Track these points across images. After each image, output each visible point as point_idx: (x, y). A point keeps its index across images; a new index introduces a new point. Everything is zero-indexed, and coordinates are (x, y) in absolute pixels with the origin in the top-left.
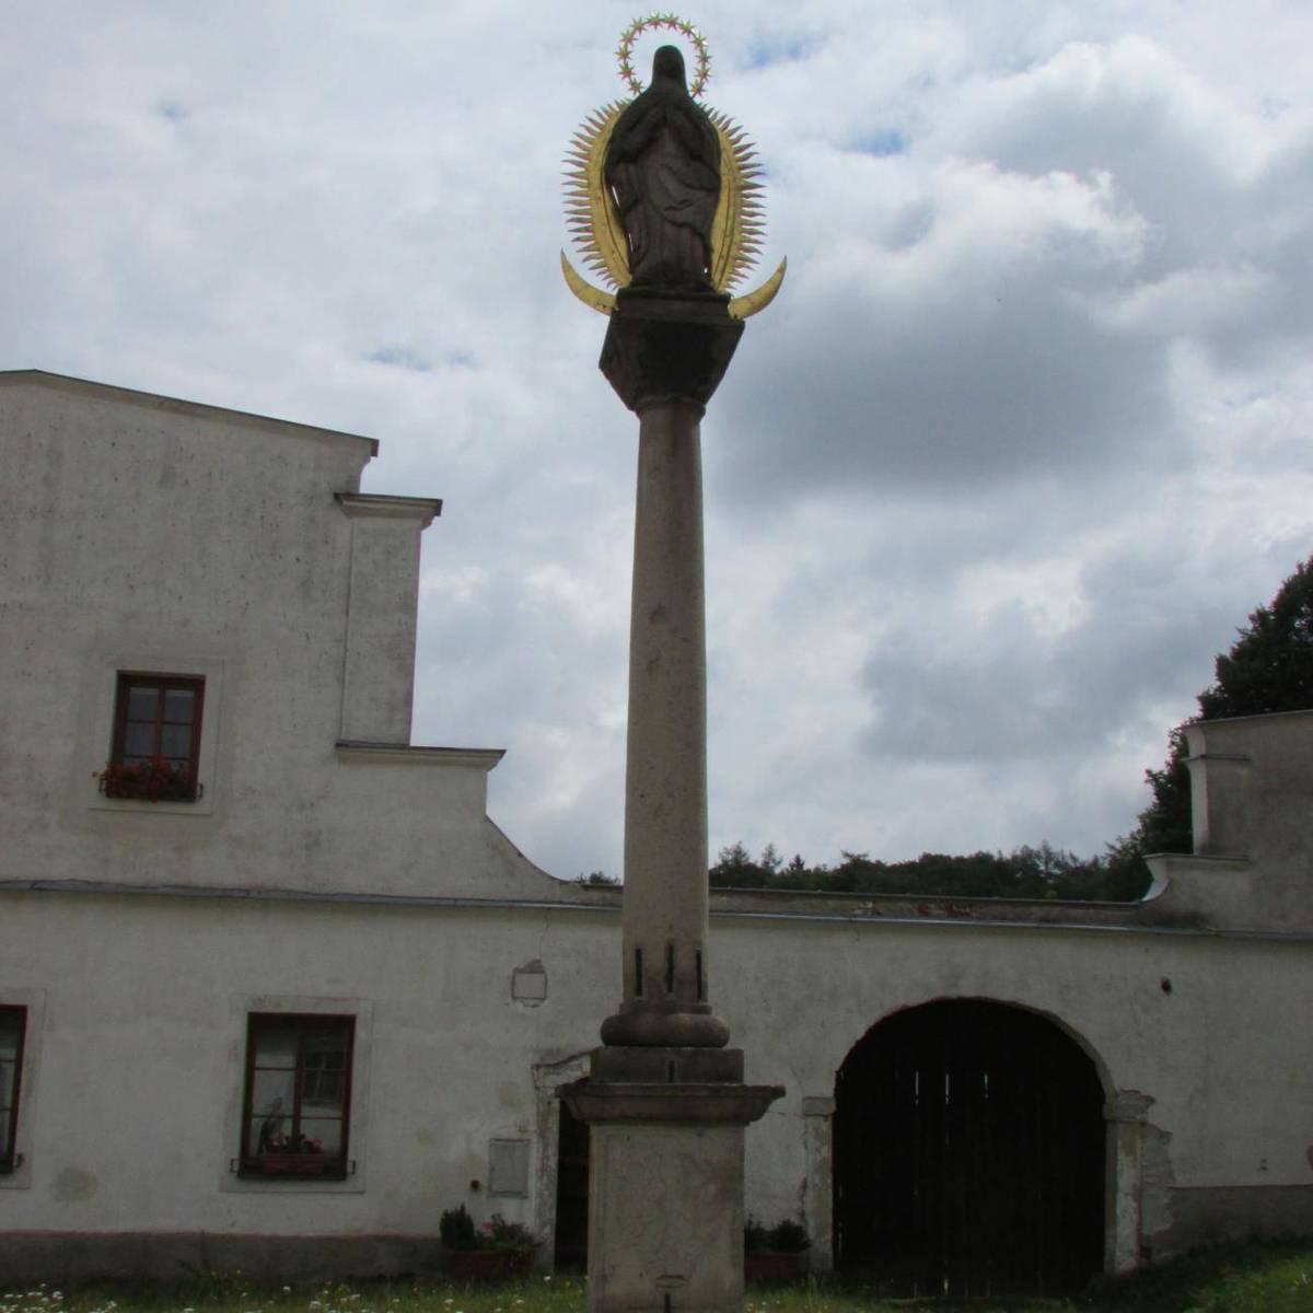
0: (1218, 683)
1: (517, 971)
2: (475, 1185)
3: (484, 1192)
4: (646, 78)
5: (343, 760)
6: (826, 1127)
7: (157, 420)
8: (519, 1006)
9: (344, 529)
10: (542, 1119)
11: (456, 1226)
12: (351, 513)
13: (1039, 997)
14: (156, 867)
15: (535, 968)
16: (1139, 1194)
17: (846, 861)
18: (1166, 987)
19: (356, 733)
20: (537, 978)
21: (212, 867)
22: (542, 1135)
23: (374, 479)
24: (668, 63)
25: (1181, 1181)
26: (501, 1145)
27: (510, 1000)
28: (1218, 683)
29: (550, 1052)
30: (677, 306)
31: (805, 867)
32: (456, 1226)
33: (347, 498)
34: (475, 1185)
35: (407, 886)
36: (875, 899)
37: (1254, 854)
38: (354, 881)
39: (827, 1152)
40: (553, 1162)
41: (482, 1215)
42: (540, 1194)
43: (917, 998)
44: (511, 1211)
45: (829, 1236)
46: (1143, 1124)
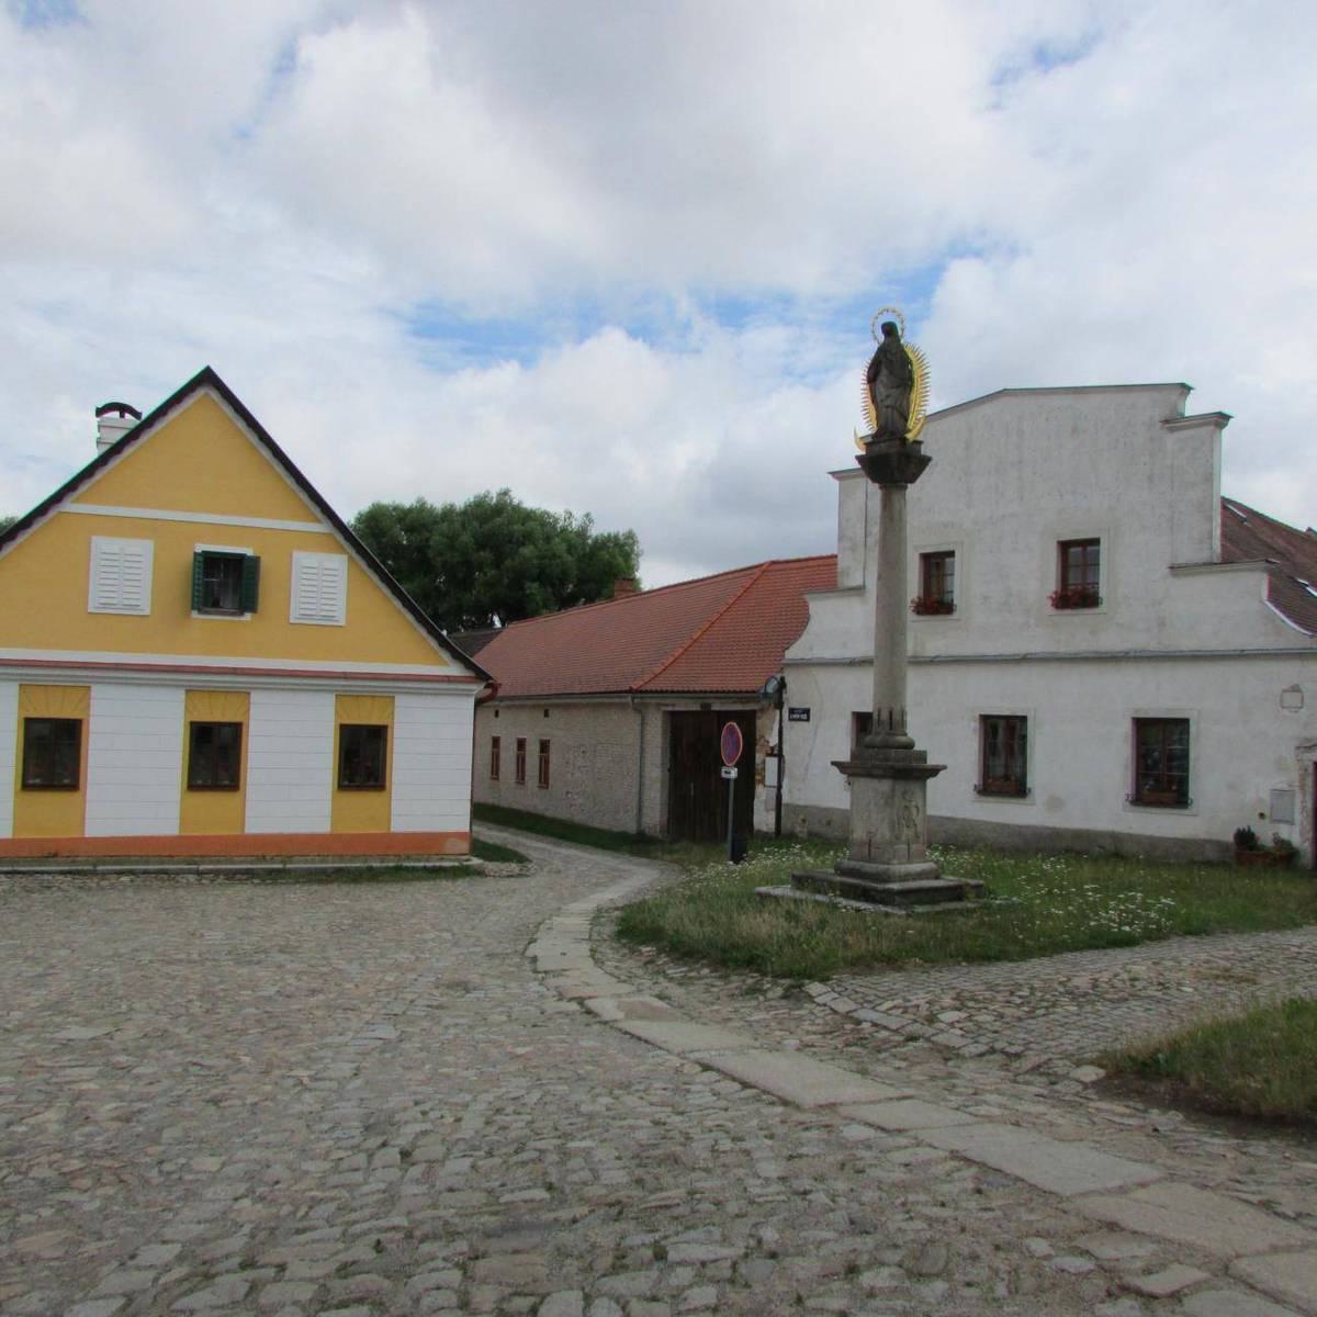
1: (1285, 691)
4: (882, 338)
5: (1175, 575)
7: (1067, 400)
8: (1286, 712)
9: (1171, 441)
12: (1172, 430)
14: (1082, 643)
15: (1295, 689)
19: (1181, 560)
20: (1298, 695)
21: (1110, 641)
22: (1302, 787)
24: (889, 330)
27: (1280, 709)
40: (1309, 805)
42: (1302, 823)
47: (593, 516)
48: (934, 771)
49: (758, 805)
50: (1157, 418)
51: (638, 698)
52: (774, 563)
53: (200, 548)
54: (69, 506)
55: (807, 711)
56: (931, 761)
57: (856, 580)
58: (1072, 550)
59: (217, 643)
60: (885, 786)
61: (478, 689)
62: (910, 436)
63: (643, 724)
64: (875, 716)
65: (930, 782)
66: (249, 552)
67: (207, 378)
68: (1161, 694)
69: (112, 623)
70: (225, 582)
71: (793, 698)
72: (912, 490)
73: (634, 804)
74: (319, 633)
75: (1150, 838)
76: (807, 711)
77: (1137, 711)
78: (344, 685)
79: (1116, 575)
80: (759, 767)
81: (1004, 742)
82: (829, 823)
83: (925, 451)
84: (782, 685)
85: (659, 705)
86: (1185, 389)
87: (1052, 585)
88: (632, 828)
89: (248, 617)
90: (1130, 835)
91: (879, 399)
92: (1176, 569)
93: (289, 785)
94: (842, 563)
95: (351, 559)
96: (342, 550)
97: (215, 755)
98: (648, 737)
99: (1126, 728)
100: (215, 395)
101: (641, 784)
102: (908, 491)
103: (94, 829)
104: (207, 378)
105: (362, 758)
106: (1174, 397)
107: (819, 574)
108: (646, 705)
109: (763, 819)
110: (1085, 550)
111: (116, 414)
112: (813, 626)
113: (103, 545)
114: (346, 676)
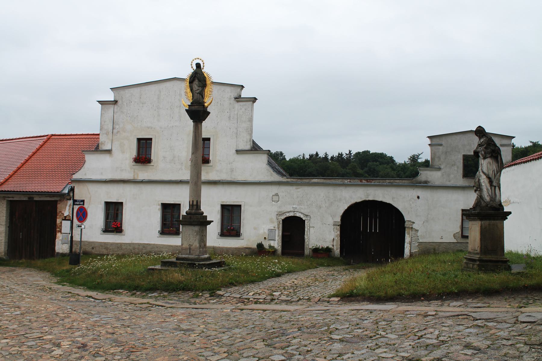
0: (288, 159)
2: (265, 238)
3: (267, 239)
4: (195, 68)
5: (237, 154)
6: (339, 227)
10: (278, 225)
11: (260, 246)
12: (238, 102)
13: (387, 200)
15: (277, 195)
16: (410, 243)
17: (531, 144)
18: (418, 197)
19: (240, 148)
22: (278, 228)
23: (245, 94)
24: (198, 66)
25: (420, 241)
26: (270, 231)
28: (288, 159)
29: (280, 212)
30: (196, 107)
31: (516, 146)
32: (260, 246)
33: (238, 99)
34: (265, 238)
35: (250, 179)
36: (350, 179)
37: (442, 167)
38: (240, 178)
39: (339, 233)
40: (281, 234)
41: (266, 245)
43: (359, 200)
44: (272, 243)
45: (339, 250)
46: (412, 228)
50: (233, 97)
52: (52, 135)
57: (108, 147)
60: (197, 228)
65: (208, 226)
72: (204, 123)
75: (226, 248)
77: (223, 202)
80: (58, 225)
81: (114, 214)
84: (72, 190)
86: (242, 87)
90: (219, 247)
91: (194, 89)
92: (238, 152)
94: (102, 139)
106: (239, 89)
107: (91, 144)
109: (61, 246)
112: (86, 165)
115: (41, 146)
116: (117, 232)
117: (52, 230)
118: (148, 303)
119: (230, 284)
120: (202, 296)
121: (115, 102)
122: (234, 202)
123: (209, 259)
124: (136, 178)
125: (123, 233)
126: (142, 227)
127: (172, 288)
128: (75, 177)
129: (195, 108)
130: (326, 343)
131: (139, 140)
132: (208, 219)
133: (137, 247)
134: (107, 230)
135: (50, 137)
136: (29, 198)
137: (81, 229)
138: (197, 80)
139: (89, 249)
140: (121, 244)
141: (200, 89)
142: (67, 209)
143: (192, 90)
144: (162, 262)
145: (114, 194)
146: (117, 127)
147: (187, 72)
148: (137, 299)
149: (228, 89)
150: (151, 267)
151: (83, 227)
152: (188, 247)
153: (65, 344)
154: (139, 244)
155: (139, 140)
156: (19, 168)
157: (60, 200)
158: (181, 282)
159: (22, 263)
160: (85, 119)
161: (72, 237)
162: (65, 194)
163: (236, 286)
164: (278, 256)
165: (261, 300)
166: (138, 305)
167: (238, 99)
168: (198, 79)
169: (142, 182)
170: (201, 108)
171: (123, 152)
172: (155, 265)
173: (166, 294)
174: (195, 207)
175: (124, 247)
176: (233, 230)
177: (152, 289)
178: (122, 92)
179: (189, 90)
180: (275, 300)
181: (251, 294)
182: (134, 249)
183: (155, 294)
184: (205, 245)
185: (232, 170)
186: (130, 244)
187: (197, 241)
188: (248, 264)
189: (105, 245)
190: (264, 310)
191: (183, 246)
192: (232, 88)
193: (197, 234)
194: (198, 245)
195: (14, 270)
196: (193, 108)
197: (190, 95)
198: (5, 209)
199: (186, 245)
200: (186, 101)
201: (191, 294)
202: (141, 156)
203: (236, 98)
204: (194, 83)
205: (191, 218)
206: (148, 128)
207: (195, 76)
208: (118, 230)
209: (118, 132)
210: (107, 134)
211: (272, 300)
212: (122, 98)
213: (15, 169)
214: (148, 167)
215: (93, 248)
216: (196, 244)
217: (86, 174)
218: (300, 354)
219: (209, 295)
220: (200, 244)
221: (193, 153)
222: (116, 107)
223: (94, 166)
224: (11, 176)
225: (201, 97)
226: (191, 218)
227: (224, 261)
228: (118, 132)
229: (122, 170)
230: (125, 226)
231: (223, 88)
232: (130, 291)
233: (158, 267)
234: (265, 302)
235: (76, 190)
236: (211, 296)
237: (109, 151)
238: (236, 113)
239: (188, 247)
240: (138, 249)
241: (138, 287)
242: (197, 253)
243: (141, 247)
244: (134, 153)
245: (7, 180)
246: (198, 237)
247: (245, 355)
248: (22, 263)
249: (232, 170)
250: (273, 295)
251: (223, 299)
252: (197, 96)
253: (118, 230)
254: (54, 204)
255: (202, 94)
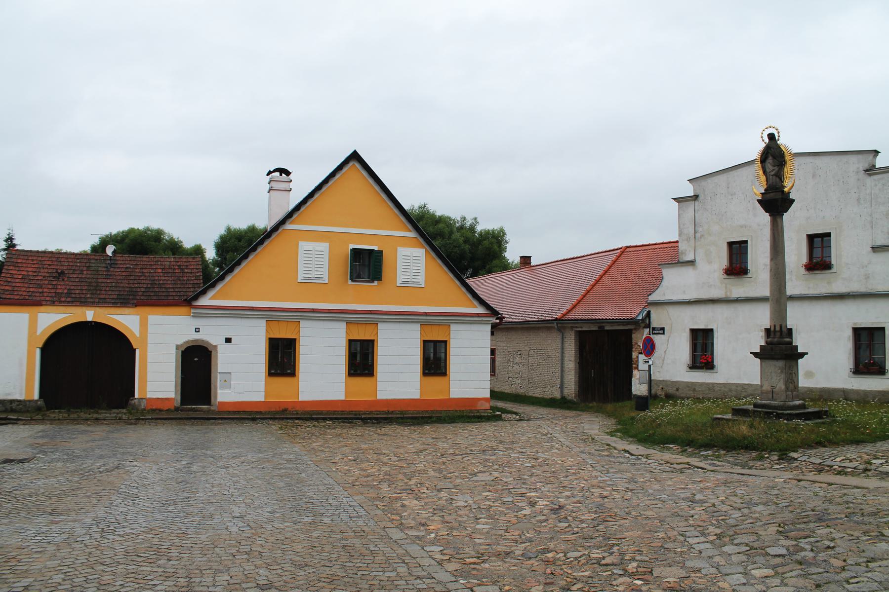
4: (767, 140)
5: (874, 252)
9: (870, 181)
12: (870, 175)
19: (879, 243)
24: (771, 137)
33: (871, 170)
47: (478, 220)
48: (802, 355)
49: (635, 381)
50: (861, 169)
51: (560, 325)
52: (628, 247)
53: (352, 246)
54: (288, 226)
55: (663, 329)
56: (800, 350)
57: (690, 257)
58: (816, 240)
59: (364, 298)
60: (781, 363)
61: (494, 320)
62: (786, 189)
63: (563, 339)
64: (772, 329)
65: (800, 361)
66: (376, 248)
67: (355, 156)
68: (868, 315)
69: (312, 286)
70: (366, 265)
71: (655, 323)
72: (786, 216)
73: (558, 382)
74: (411, 290)
75: (863, 391)
76: (663, 329)
77: (855, 324)
78: (425, 319)
79: (842, 252)
80: (634, 360)
81: (702, 345)
82: (677, 390)
83: (791, 196)
84: (649, 314)
85: (572, 327)
86: (876, 152)
87: (804, 260)
88: (557, 395)
89: (376, 283)
90: (853, 390)
91: (768, 170)
92: (875, 249)
93: (399, 376)
94: (682, 246)
95: (426, 251)
96: (423, 247)
97: (361, 360)
98: (566, 345)
99: (850, 333)
100: (358, 165)
101: (562, 371)
102: (784, 217)
103: (304, 397)
104: (355, 156)
105: (434, 362)
106: (871, 157)
107: (667, 255)
108: (564, 328)
109: (639, 388)
110: (822, 240)
111: (278, 174)
112: (665, 283)
113: (305, 246)
114: (426, 314)
115: (614, 262)
116: (707, 369)
117: (628, 366)
118: (688, 463)
119: (816, 443)
120: (768, 458)
121: (696, 197)
122: (873, 323)
123: (803, 406)
124: (729, 295)
125: (715, 370)
126: (738, 363)
127: (733, 445)
128: (652, 298)
129: (771, 196)
130: (868, 540)
131: (730, 244)
132: (799, 351)
133: (734, 388)
134: (694, 366)
135: (624, 250)
136: (599, 327)
137: (650, 366)
138: (770, 158)
139: (671, 391)
140: (713, 384)
141: (776, 168)
142: (639, 338)
143: (764, 172)
144: (733, 409)
145: (701, 318)
146: (700, 229)
147: (755, 148)
148: (674, 456)
149: (853, 159)
150: (719, 416)
151: (650, 362)
152: (769, 389)
153: (541, 503)
154: (737, 385)
155: (730, 244)
156: (588, 292)
157: (635, 329)
158: (745, 438)
159: (591, 408)
160: (658, 225)
161: (650, 375)
162: (638, 321)
163: (825, 447)
164: (662, 400)
165: (849, 470)
166: (675, 466)
167: (871, 170)
168: (773, 155)
169: (737, 301)
170: (779, 196)
171: (710, 262)
172: (726, 413)
173: (722, 452)
174: (778, 334)
175: (717, 389)
176: (874, 364)
177: (707, 446)
178: (703, 183)
179: (761, 172)
180: (869, 470)
181: (838, 459)
182: (730, 390)
183: (710, 452)
184: (796, 387)
185: (867, 277)
186: (724, 385)
187: (782, 381)
188: (860, 416)
189: (692, 386)
190: (830, 484)
191: (764, 388)
192: (860, 156)
193: (782, 372)
194: (783, 387)
195: (580, 415)
196: (769, 196)
197: (763, 178)
198: (573, 341)
199: (766, 387)
200: (759, 188)
201: (754, 454)
202: (734, 265)
203: (866, 171)
204: (767, 161)
205: (772, 350)
206: (741, 227)
207: (768, 153)
208: (709, 365)
209: (702, 236)
210: (688, 240)
211: (866, 470)
212: (704, 190)
213: (583, 292)
214: (744, 280)
215: (677, 390)
216: (781, 386)
217: (664, 294)
218: (812, 550)
219: (776, 458)
220: (786, 383)
221: (772, 260)
222: (697, 203)
223: (675, 284)
224: (579, 302)
225: (778, 180)
226: (772, 350)
227: (827, 411)
228: (702, 236)
229: (710, 286)
230: (718, 360)
231: (845, 158)
232: (682, 446)
233: (729, 416)
234: (854, 473)
235: (653, 316)
236: (779, 459)
237: (692, 263)
238: (868, 192)
239: (769, 389)
240: (736, 391)
241: (692, 442)
242: (783, 398)
243: (739, 388)
244: (724, 262)
245: (574, 306)
246: (783, 376)
247: (735, 542)
248: (591, 408)
249: (867, 277)
250: (870, 464)
251: (794, 465)
252: (773, 180)
253: (709, 365)
254: (628, 334)
255: (780, 176)
